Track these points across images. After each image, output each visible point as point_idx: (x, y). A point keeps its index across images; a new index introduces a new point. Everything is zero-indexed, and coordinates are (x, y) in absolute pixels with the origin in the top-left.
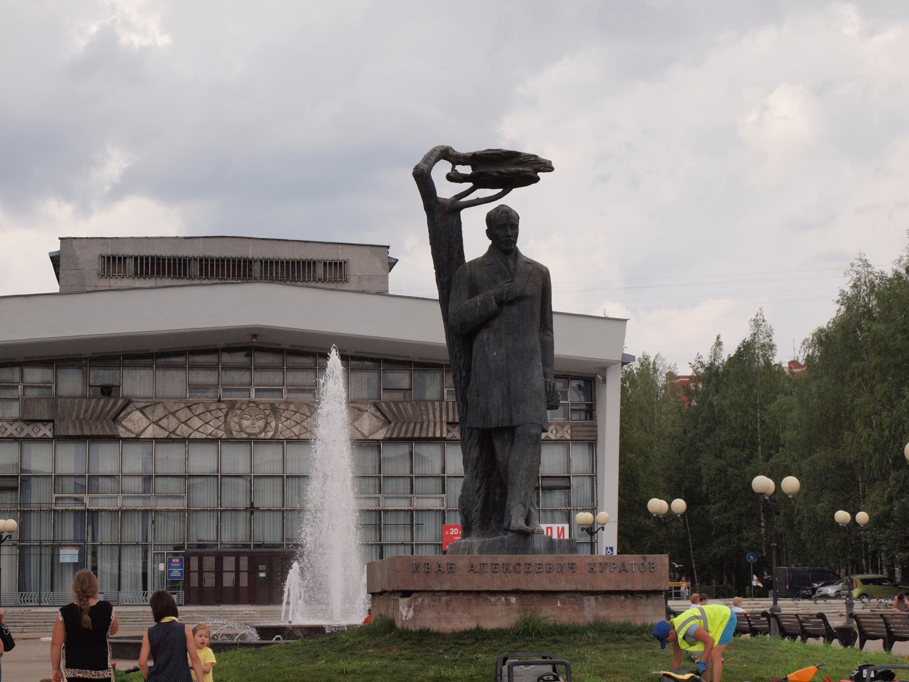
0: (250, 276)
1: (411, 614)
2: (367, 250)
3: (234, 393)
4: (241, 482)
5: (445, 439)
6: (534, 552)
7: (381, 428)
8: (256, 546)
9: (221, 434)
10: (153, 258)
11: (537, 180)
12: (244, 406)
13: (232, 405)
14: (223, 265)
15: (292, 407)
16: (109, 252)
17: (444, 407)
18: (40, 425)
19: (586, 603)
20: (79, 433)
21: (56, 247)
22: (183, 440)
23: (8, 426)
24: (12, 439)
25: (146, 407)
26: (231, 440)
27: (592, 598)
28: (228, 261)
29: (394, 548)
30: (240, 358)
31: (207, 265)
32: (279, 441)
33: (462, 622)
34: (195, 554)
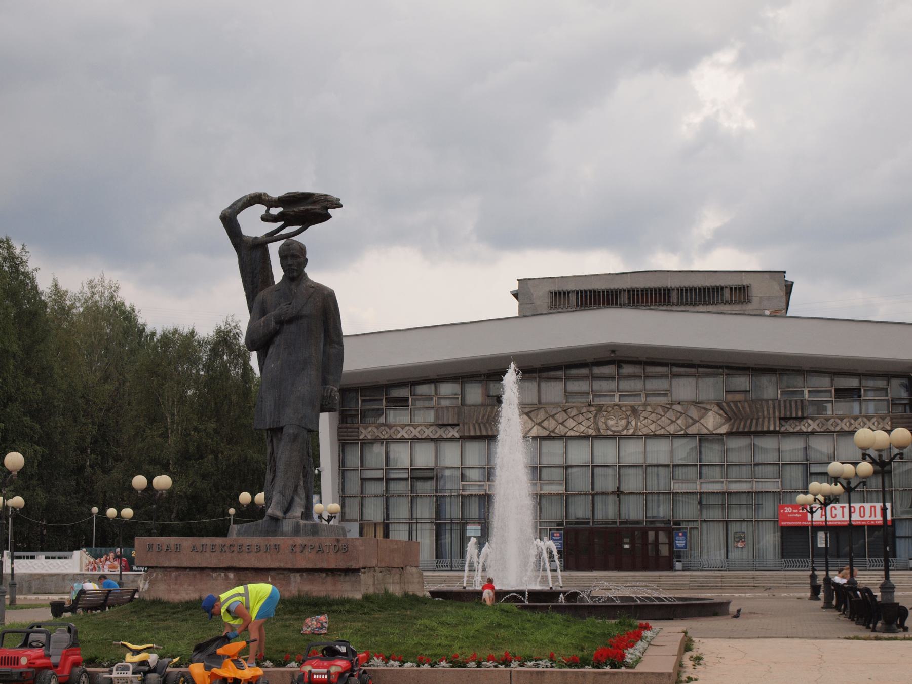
0: (669, 301)
1: (147, 586)
2: (767, 276)
3: (602, 398)
4: (610, 471)
5: (778, 432)
6: (283, 534)
7: (724, 424)
8: (621, 523)
9: (591, 432)
10: (590, 292)
11: (328, 217)
12: (610, 409)
13: (600, 408)
14: (647, 294)
15: (649, 409)
16: (556, 288)
17: (776, 405)
18: (449, 428)
19: (293, 579)
20: (478, 434)
21: (516, 287)
22: (561, 437)
23: (426, 430)
24: (428, 439)
25: (531, 412)
26: (599, 437)
27: (298, 575)
28: (651, 290)
29: (738, 524)
30: (637, 370)
31: (634, 295)
32: (639, 437)
33: (187, 594)
34: (652, 529)
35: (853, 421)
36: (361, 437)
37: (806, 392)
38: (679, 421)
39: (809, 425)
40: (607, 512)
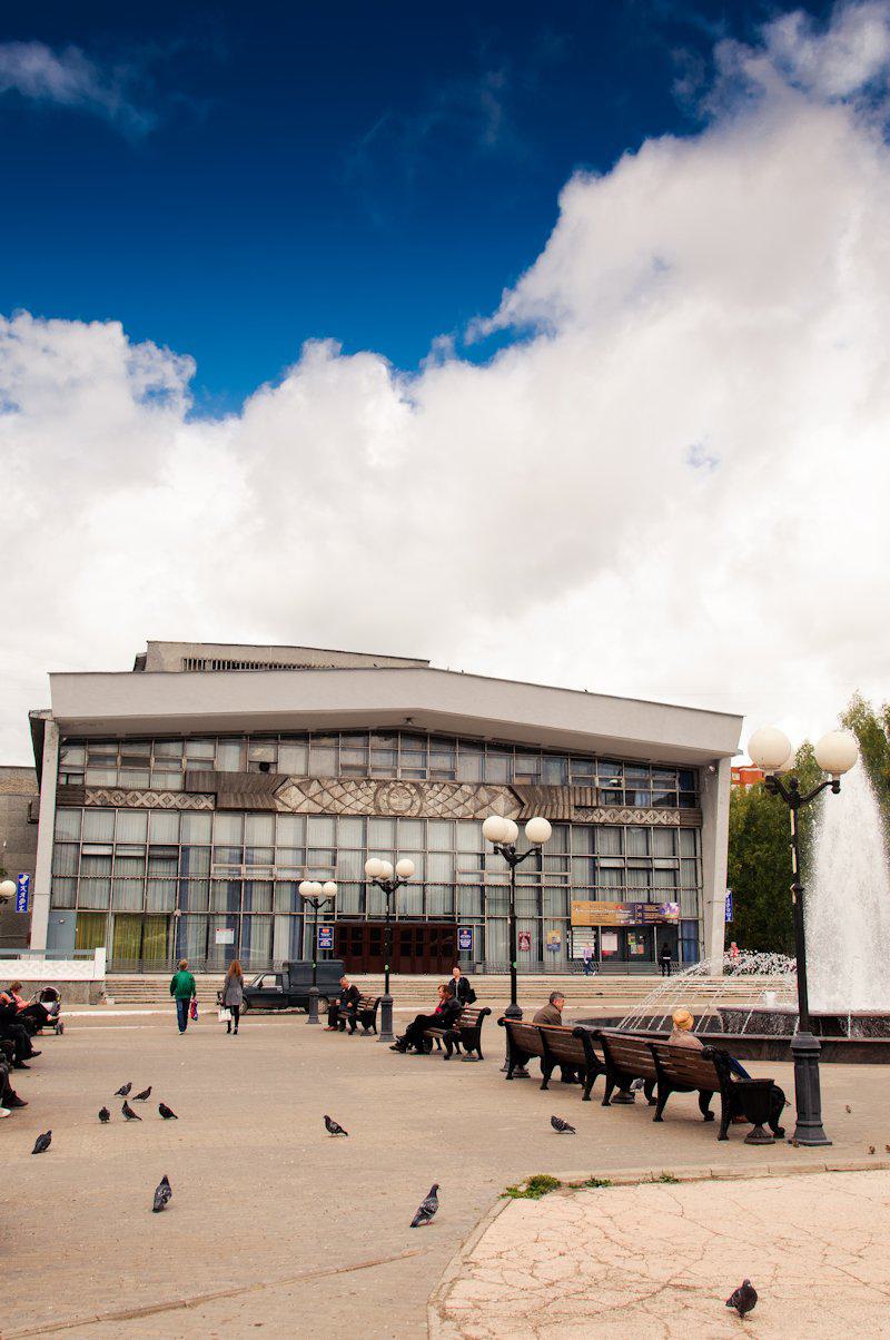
7: (514, 809)
9: (371, 810)
23: (608, 818)
35: (643, 814)
36: (87, 803)
37: (597, 780)
38: (467, 804)
39: (601, 815)
40: (377, 905)
